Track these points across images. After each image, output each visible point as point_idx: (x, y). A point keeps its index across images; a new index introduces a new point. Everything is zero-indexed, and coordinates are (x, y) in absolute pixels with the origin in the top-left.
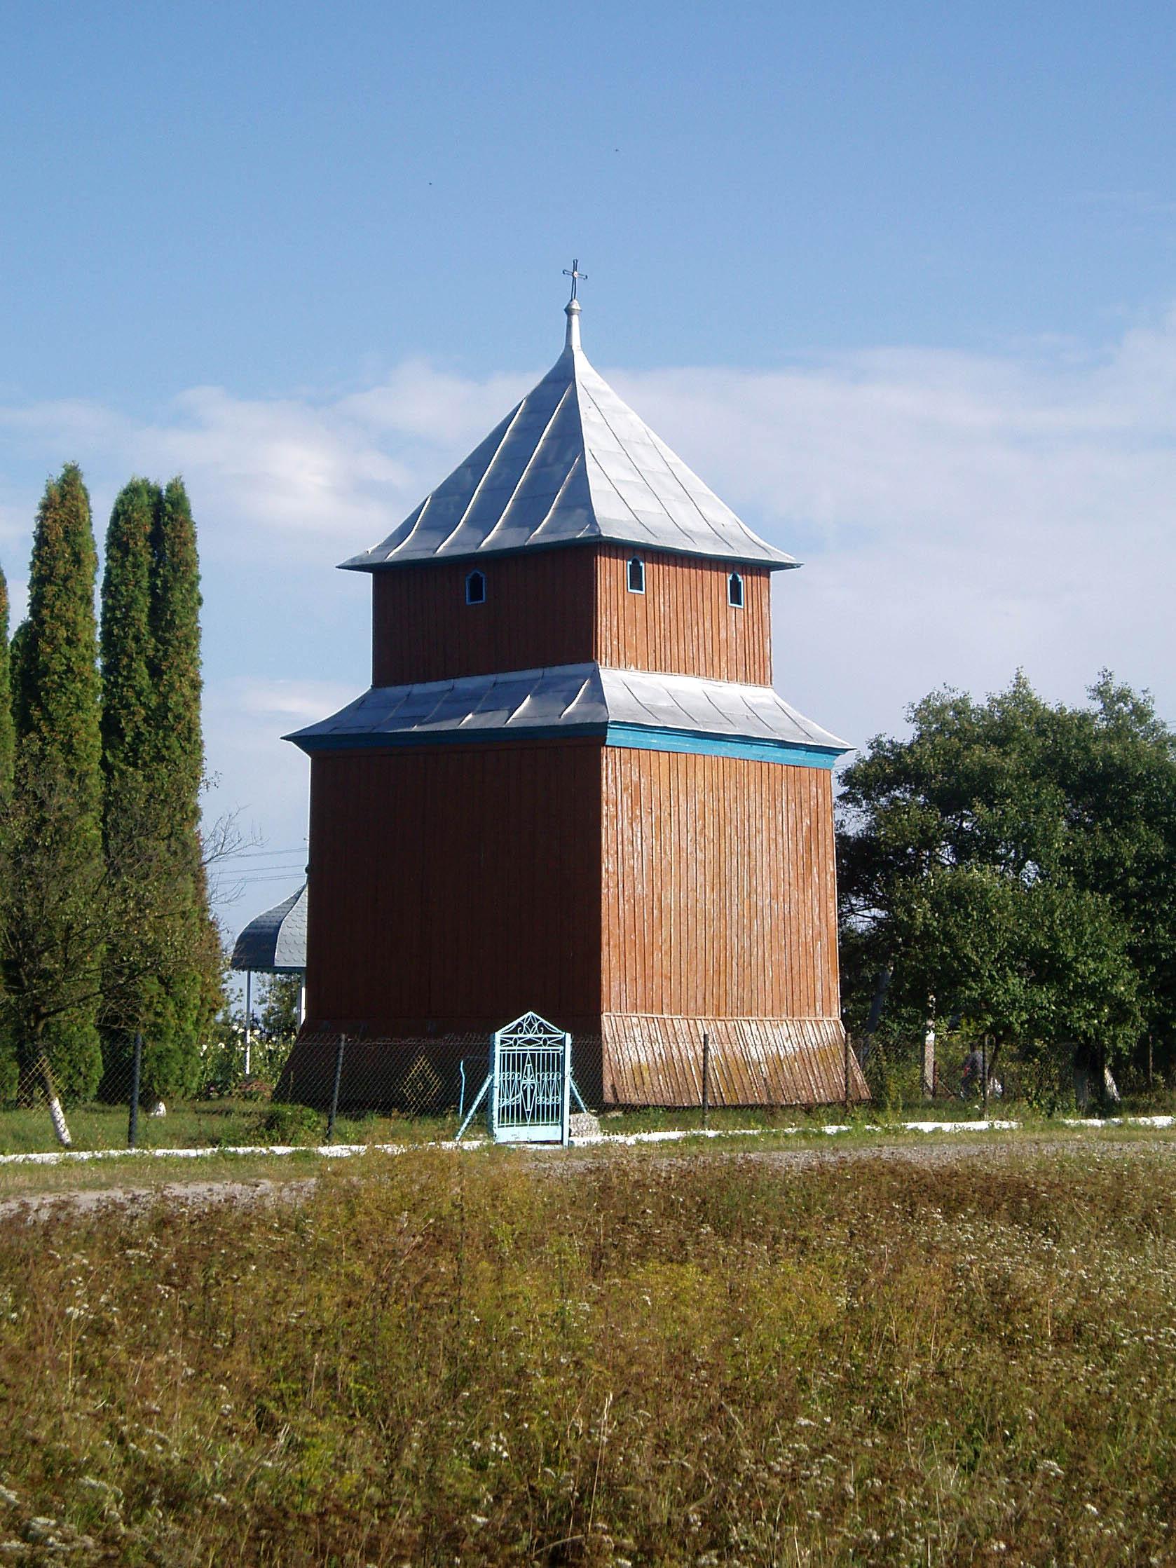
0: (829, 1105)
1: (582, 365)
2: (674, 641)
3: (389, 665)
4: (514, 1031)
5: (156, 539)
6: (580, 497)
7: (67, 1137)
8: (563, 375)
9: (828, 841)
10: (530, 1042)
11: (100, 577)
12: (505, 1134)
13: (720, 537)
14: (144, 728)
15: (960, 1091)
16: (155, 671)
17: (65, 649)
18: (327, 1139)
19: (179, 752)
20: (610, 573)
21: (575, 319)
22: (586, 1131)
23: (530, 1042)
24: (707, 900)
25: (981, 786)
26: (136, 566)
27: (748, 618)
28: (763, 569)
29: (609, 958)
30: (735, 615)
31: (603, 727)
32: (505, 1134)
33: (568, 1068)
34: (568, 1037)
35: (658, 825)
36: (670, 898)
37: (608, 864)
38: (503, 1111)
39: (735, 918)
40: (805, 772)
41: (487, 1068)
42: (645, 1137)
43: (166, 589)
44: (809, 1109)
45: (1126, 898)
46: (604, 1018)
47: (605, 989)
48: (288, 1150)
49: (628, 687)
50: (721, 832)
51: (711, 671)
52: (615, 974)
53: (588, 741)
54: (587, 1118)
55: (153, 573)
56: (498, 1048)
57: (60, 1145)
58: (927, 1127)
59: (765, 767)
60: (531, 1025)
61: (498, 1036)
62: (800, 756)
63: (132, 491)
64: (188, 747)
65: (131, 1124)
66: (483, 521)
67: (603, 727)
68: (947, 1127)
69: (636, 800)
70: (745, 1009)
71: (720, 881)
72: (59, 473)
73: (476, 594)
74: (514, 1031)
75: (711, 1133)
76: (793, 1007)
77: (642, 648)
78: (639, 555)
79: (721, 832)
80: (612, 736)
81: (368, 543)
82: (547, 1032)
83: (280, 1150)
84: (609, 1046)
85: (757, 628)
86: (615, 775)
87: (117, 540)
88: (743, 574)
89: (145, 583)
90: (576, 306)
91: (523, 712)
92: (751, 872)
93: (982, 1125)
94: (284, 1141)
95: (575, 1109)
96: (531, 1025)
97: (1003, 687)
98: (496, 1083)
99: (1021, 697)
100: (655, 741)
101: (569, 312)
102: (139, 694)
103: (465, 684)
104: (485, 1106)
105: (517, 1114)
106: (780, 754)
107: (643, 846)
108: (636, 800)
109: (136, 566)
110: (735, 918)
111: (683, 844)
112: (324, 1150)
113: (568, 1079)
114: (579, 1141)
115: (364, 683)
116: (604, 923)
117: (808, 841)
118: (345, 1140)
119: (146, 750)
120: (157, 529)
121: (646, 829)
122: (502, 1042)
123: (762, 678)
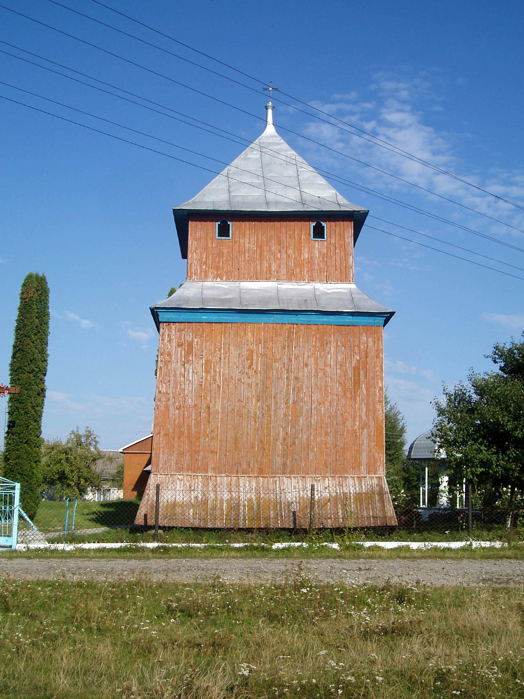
24: (253, 406)
30: (318, 245)
34: (18, 485)
50: (268, 367)
51: (291, 277)
54: (34, 531)
70: (287, 470)
106: (326, 319)
117: (356, 370)
123: (344, 278)
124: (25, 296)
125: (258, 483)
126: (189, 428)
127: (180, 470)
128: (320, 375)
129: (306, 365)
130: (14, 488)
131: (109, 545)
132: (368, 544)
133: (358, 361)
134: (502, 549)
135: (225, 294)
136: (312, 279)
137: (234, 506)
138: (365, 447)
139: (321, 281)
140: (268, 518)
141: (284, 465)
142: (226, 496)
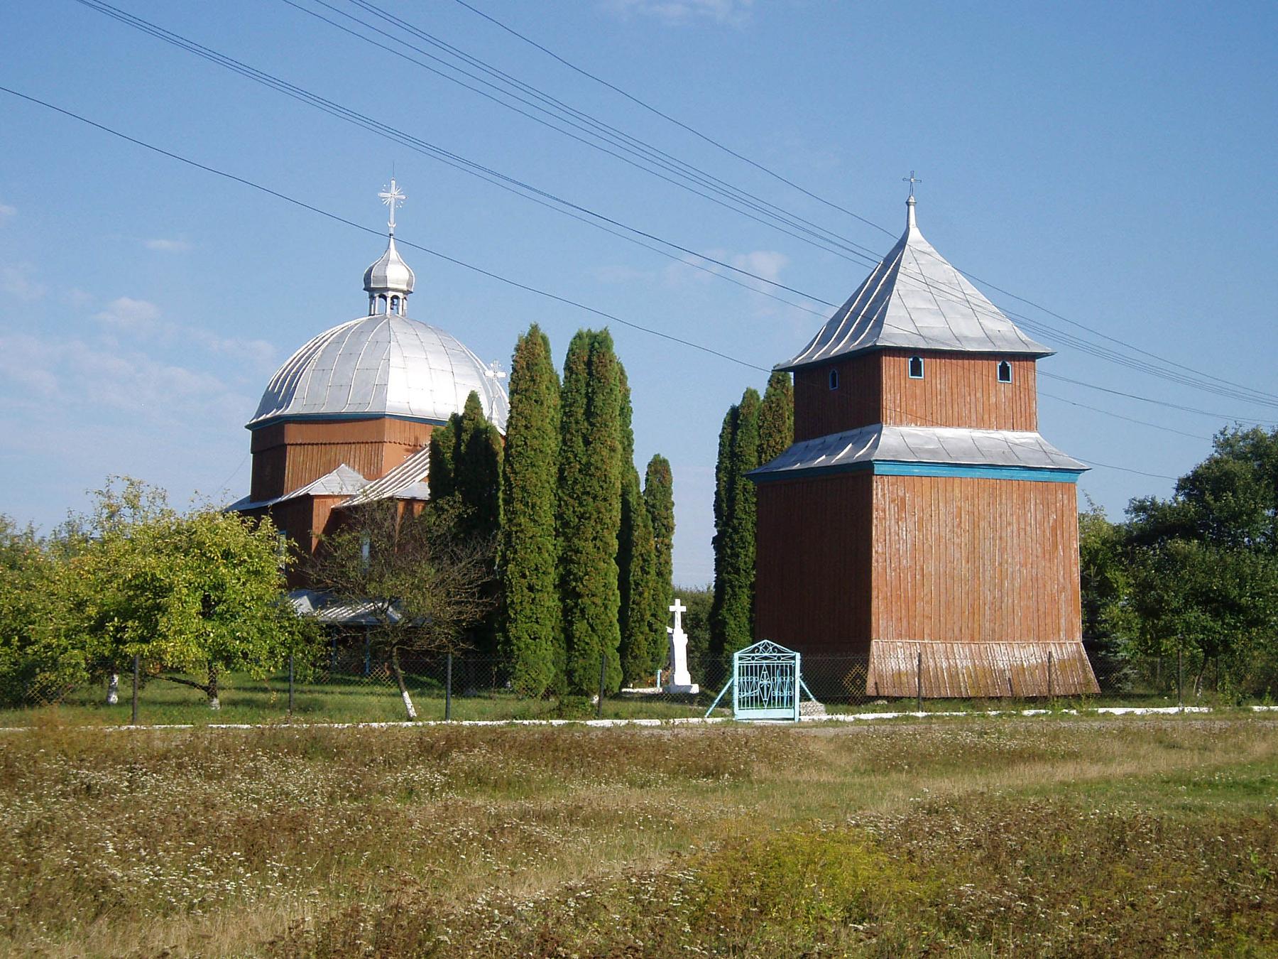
0: (1065, 697)
1: (915, 234)
2: (949, 406)
4: (753, 651)
5: (589, 364)
7: (412, 713)
9: (1072, 528)
10: (766, 658)
13: (1004, 339)
14: (577, 475)
16: (587, 443)
19: (598, 488)
20: (893, 372)
21: (912, 208)
22: (816, 712)
23: (766, 658)
24: (964, 569)
26: (577, 381)
28: (1032, 357)
30: (1005, 388)
32: (742, 714)
34: (798, 655)
35: (920, 524)
36: (931, 567)
37: (877, 548)
39: (988, 579)
40: (1052, 486)
42: (863, 716)
46: (873, 643)
47: (874, 625)
48: (561, 722)
49: (897, 437)
50: (975, 525)
51: (981, 424)
53: (862, 473)
54: (814, 704)
55: (588, 385)
56: (736, 663)
57: (410, 719)
59: (1015, 484)
60: (766, 648)
62: (1047, 475)
63: (579, 336)
64: (605, 486)
65: (999, 699)
66: (855, 337)
68: (1138, 711)
70: (996, 636)
71: (973, 554)
72: (526, 330)
73: (834, 385)
74: (753, 651)
75: (920, 714)
76: (1039, 635)
78: (916, 357)
80: (878, 469)
82: (779, 651)
86: (881, 493)
87: (568, 368)
88: (1006, 362)
89: (583, 392)
90: (912, 200)
91: (842, 456)
92: (1002, 551)
94: (560, 717)
95: (804, 697)
96: (766, 648)
98: (736, 683)
100: (916, 470)
101: (908, 204)
102: (576, 456)
105: (755, 702)
106: (1026, 474)
107: (899, 536)
109: (577, 381)
110: (988, 579)
111: (943, 534)
114: (805, 719)
115: (247, 492)
116: (874, 584)
117: (1054, 529)
118: (617, 716)
120: (592, 355)
121: (911, 526)
122: (740, 659)
123: (1029, 428)
124: (974, 424)
125: (971, 650)
126: (906, 591)
127: (900, 636)
128: (1022, 534)
129: (1009, 524)
130: (794, 658)
131: (885, 715)
132: (1101, 710)
133: (1056, 521)
134: (1209, 713)
135: (926, 443)
136: (999, 428)
137: (954, 675)
138: (1063, 612)
139: (1008, 429)
140: (986, 686)
141: (994, 631)
142: (945, 665)
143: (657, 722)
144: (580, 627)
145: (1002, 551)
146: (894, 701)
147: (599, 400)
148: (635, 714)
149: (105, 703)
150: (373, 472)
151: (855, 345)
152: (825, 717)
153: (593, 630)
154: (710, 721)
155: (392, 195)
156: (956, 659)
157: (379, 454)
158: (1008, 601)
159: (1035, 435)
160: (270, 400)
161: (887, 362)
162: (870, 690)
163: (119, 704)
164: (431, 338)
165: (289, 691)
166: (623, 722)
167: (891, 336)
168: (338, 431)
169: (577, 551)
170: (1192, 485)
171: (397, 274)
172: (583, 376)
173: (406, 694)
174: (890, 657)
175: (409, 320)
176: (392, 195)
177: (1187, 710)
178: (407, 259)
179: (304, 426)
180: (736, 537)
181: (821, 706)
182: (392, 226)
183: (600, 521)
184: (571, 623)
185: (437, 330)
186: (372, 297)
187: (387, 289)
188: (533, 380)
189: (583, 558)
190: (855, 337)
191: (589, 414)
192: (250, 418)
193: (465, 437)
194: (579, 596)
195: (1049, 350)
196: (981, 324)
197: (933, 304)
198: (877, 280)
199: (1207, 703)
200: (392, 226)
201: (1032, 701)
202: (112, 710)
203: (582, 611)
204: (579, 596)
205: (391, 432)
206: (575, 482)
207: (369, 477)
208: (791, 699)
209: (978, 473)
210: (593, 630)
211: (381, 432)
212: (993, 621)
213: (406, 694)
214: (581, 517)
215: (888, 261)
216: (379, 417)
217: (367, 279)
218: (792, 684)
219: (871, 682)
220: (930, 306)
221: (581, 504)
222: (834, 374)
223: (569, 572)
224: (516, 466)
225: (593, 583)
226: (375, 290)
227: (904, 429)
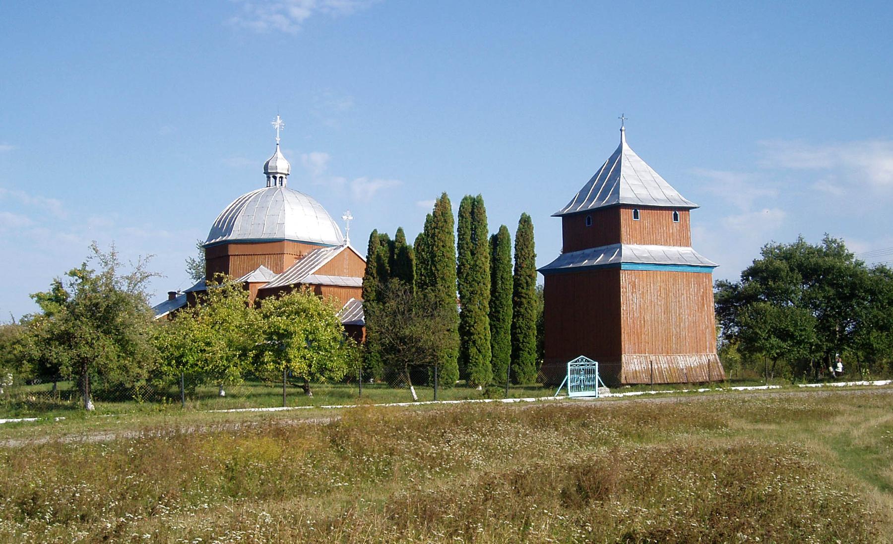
1: (625, 146)
3: (569, 246)
5: (472, 213)
6: (617, 191)
8: (619, 151)
11: (456, 226)
12: (572, 394)
15: (765, 375)
16: (473, 254)
17: (442, 248)
18: (506, 397)
20: (626, 216)
22: (605, 393)
25: (775, 275)
27: (681, 226)
28: (687, 209)
29: (624, 337)
30: (676, 225)
31: (620, 264)
32: (572, 394)
33: (597, 373)
34: (597, 363)
36: (648, 318)
37: (623, 308)
38: (572, 387)
41: (566, 374)
43: (476, 228)
44: (694, 384)
45: (807, 314)
50: (667, 295)
51: (666, 243)
52: (627, 342)
53: (615, 269)
54: (605, 389)
56: (569, 368)
58: (741, 388)
61: (569, 364)
62: (699, 269)
63: (465, 199)
67: (620, 264)
68: (749, 388)
69: (634, 286)
70: (679, 352)
71: (667, 311)
73: (589, 223)
75: (653, 392)
77: (639, 237)
78: (636, 208)
79: (667, 295)
80: (623, 267)
81: (561, 208)
83: (487, 401)
84: (624, 366)
85: (685, 228)
87: (461, 215)
88: (677, 211)
91: (600, 260)
93: (765, 387)
94: (489, 398)
95: (600, 385)
97: (793, 240)
99: (800, 245)
100: (640, 267)
103: (587, 251)
104: (566, 385)
105: (578, 388)
106: (690, 269)
107: (635, 302)
108: (634, 286)
112: (505, 401)
113: (597, 377)
114: (601, 396)
117: (702, 296)
118: (513, 396)
119: (470, 279)
123: (687, 246)
127: (635, 353)
143: (534, 399)
144: (473, 351)
145: (680, 308)
146: (634, 386)
147: (479, 231)
148: (523, 396)
149: (219, 396)
150: (278, 269)
151: (603, 203)
152: (610, 395)
153: (480, 352)
154: (558, 398)
155: (278, 123)
156: (662, 363)
157: (281, 260)
158: (683, 333)
159: (690, 249)
160: (215, 231)
161: (622, 211)
162: (623, 381)
163: (225, 397)
164: (304, 199)
165: (283, 387)
166: (518, 400)
167: (625, 198)
168: (258, 248)
169: (469, 311)
170: (752, 273)
171: (282, 165)
172: (469, 219)
173: (412, 388)
174: (632, 363)
175: (289, 189)
176: (278, 123)
177: (771, 387)
178: (286, 157)
179: (239, 246)
180: (497, 302)
181: (608, 389)
182: (278, 139)
183: (482, 295)
184: (468, 349)
185: (306, 195)
186: (269, 178)
187: (277, 173)
188: (445, 221)
189: (474, 314)
190: (602, 198)
191: (473, 239)
192: (204, 239)
193: (396, 251)
194: (472, 334)
195: (696, 205)
196: (665, 193)
197: (639, 183)
198: (607, 169)
199: (779, 384)
200: (278, 139)
201: (702, 384)
202: (222, 400)
203: (474, 342)
204: (472, 334)
205: (288, 248)
206: (468, 275)
207: (276, 272)
208: (594, 386)
209: (668, 268)
210: (480, 352)
211: (282, 248)
212: (677, 344)
213: (412, 388)
214: (472, 293)
215: (612, 160)
216: (284, 240)
217: (266, 167)
218: (595, 378)
219: (623, 376)
220: (636, 183)
221: (471, 286)
222: (589, 219)
223: (466, 322)
224: (438, 267)
225: (479, 328)
226: (270, 174)
227: (631, 246)
